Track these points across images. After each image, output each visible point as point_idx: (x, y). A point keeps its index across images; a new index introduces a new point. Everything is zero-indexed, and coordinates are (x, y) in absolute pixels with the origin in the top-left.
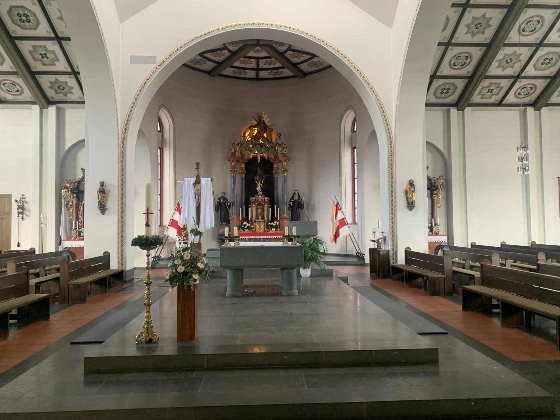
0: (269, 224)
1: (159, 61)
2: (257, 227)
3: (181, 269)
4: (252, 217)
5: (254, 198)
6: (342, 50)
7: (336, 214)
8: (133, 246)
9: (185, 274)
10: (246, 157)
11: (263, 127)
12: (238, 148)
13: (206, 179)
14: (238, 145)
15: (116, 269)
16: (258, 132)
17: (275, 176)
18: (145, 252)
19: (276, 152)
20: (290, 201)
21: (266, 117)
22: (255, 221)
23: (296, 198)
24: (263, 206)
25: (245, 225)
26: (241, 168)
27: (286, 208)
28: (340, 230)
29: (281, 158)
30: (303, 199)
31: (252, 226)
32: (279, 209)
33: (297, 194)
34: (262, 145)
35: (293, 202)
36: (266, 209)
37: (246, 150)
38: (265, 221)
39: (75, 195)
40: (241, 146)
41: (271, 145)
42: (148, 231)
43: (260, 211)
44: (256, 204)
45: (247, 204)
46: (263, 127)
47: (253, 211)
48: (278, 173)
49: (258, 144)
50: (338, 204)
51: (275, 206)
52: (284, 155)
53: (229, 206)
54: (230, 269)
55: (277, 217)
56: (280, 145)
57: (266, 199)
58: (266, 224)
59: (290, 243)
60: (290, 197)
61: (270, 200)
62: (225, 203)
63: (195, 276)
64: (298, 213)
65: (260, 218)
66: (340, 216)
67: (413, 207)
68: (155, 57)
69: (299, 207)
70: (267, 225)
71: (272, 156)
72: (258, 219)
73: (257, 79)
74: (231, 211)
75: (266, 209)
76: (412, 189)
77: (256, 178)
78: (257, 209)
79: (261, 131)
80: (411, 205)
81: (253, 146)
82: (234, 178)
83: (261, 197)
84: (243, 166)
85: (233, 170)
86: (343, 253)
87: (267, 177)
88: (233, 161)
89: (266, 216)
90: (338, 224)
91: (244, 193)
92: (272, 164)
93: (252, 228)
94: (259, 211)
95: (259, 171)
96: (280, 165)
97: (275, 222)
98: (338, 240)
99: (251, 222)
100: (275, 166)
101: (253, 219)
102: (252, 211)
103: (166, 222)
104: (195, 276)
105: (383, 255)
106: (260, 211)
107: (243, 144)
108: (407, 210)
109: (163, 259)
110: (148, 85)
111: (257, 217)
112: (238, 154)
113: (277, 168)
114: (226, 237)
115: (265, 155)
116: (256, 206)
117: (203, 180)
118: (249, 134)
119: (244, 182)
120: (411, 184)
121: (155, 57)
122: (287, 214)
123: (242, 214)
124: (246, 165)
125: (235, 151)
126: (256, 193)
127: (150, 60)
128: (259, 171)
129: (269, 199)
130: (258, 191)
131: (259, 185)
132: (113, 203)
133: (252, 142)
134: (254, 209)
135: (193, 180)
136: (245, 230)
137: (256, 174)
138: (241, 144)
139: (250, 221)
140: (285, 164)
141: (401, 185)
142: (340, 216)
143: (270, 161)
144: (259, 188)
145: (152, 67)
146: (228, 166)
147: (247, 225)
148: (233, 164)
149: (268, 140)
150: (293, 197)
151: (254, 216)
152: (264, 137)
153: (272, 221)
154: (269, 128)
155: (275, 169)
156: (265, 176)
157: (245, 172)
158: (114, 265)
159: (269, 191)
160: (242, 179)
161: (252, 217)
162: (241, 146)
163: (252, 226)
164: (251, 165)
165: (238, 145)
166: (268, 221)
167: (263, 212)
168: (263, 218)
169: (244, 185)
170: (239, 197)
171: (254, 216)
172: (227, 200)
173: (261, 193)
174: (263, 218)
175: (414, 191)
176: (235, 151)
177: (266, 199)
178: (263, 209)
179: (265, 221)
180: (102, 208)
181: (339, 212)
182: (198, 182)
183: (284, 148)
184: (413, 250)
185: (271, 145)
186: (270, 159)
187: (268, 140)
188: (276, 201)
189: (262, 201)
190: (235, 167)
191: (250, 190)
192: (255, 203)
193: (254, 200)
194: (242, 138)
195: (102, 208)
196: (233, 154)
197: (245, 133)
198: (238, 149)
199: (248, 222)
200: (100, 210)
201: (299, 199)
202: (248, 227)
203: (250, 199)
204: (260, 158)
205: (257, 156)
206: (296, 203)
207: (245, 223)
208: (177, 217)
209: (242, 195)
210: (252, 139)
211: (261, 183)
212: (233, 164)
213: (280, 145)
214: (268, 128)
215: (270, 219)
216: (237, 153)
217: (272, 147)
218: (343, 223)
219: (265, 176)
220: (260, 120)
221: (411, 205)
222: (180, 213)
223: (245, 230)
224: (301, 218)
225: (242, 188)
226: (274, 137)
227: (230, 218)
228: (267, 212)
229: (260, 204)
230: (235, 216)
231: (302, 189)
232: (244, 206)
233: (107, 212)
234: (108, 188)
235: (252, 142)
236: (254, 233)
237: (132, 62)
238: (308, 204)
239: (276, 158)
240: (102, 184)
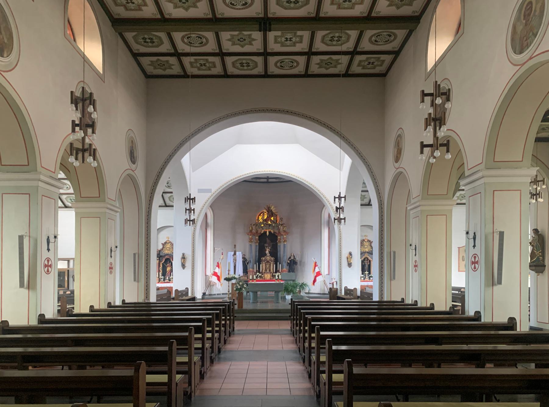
0: (274, 274)
1: (213, 191)
2: (266, 276)
3: (239, 287)
4: (263, 270)
5: (264, 258)
6: (313, 184)
7: (315, 268)
8: (226, 281)
9: (240, 288)
10: (259, 232)
11: (271, 213)
12: (254, 227)
13: (239, 252)
14: (254, 225)
15: (465, 210)
16: (267, 217)
17: (278, 244)
18: (228, 282)
19: (279, 229)
20: (288, 260)
21: (273, 207)
22: (265, 273)
23: (292, 258)
24: (270, 263)
25: (258, 275)
26: (256, 239)
27: (285, 265)
28: (317, 278)
29: (282, 233)
30: (297, 259)
31: (263, 276)
32: (280, 265)
33: (293, 255)
34: (270, 225)
35: (290, 261)
36: (272, 265)
37: (259, 228)
38: (271, 273)
39: (158, 258)
40: (256, 226)
41: (276, 225)
42: (229, 276)
43: (268, 266)
44: (266, 262)
45: (259, 262)
46: (271, 213)
47: (263, 266)
48: (281, 242)
49: (268, 224)
50: (316, 263)
51: (278, 263)
52: (285, 231)
53: (248, 263)
54: (252, 292)
55: (279, 270)
56: (282, 225)
57: (272, 258)
58: (272, 274)
59: (278, 282)
60: (289, 257)
61: (275, 259)
62: (245, 261)
63: (243, 289)
64: (293, 267)
65: (268, 271)
66: (317, 270)
67: (351, 266)
68: (211, 190)
69: (294, 264)
70: (273, 275)
71: (277, 231)
72: (266, 271)
73: (268, 182)
74: (248, 266)
75: (272, 265)
76: (351, 257)
77: (266, 245)
78: (266, 265)
79: (270, 216)
80: (350, 265)
81: (264, 225)
82: (251, 245)
83: (268, 258)
84: (257, 238)
85: (251, 241)
86: (322, 293)
87: (273, 245)
88: (251, 235)
89: (272, 269)
90: (315, 275)
91: (257, 255)
92: (277, 236)
93: (262, 277)
94: (267, 266)
95: (268, 241)
96: (282, 237)
97: (278, 273)
98: (315, 283)
99: (262, 273)
100: (279, 237)
101: (263, 271)
102: (263, 266)
103: (209, 273)
104: (243, 289)
105: (334, 291)
106: (268, 266)
107: (257, 225)
108: (348, 267)
109: (207, 295)
110: (207, 204)
111: (266, 270)
112: (254, 231)
113: (280, 239)
114: (251, 279)
115: (272, 231)
116: (266, 263)
117: (237, 253)
118: (262, 218)
119: (258, 247)
120: (350, 254)
121: (211, 190)
122: (286, 268)
123: (256, 268)
124: (259, 237)
125: (252, 229)
126: (266, 255)
127: (209, 191)
128: (268, 241)
129: (274, 259)
130: (267, 253)
131: (268, 250)
132: (188, 264)
133: (263, 223)
134: (264, 265)
135: (233, 253)
136: (258, 278)
137: (265, 243)
138: (256, 225)
139: (261, 272)
140: (285, 237)
141: (345, 254)
142: (317, 270)
143: (275, 235)
144: (267, 252)
145: (210, 194)
146: (247, 237)
147: (259, 275)
148: (251, 237)
149: (274, 222)
150: (290, 258)
151: (264, 270)
152: (271, 220)
153: (276, 272)
154: (275, 214)
155: (278, 240)
156: (272, 244)
157: (259, 241)
158: (190, 294)
159: (275, 254)
160: (256, 246)
161: (263, 270)
162: (256, 226)
163: (263, 276)
164: (262, 238)
165: (254, 225)
166: (273, 272)
167: (270, 267)
168: (270, 270)
169: (258, 250)
170: (254, 257)
171: (264, 270)
172: (246, 259)
173: (269, 255)
174: (270, 270)
175: (351, 258)
176: (252, 229)
177: (272, 258)
178: (270, 265)
179: (271, 273)
180: (183, 266)
181: (317, 268)
182: (235, 254)
183: (284, 227)
184: (349, 288)
185: (276, 225)
186: (276, 233)
187: (274, 222)
188: (279, 260)
189: (269, 260)
190: (252, 239)
191: (261, 253)
192: (265, 261)
193: (264, 260)
194: (257, 221)
195: (183, 266)
196: (251, 231)
197: (258, 218)
198: (254, 228)
199: (260, 273)
200: (182, 267)
201: (294, 259)
202: (260, 277)
203: (262, 258)
204: (269, 232)
205: (267, 231)
206: (292, 262)
207: (258, 274)
208: (217, 270)
209: (256, 256)
210: (263, 221)
211: (269, 248)
212: (251, 237)
213: (282, 225)
214: (274, 214)
215: (274, 271)
216: (253, 230)
217: (277, 226)
218: (319, 274)
219: (272, 244)
220: (269, 209)
221: (350, 265)
222: (219, 268)
223: (258, 278)
224: (295, 270)
225: (256, 251)
226: (278, 219)
227: (248, 270)
228: (273, 267)
229: (268, 262)
230: (251, 269)
231: (296, 252)
232: (257, 263)
233: (186, 268)
234: (186, 256)
235: (263, 223)
236: (264, 280)
237: (198, 192)
238: (301, 262)
239: (279, 232)
240: (183, 254)
